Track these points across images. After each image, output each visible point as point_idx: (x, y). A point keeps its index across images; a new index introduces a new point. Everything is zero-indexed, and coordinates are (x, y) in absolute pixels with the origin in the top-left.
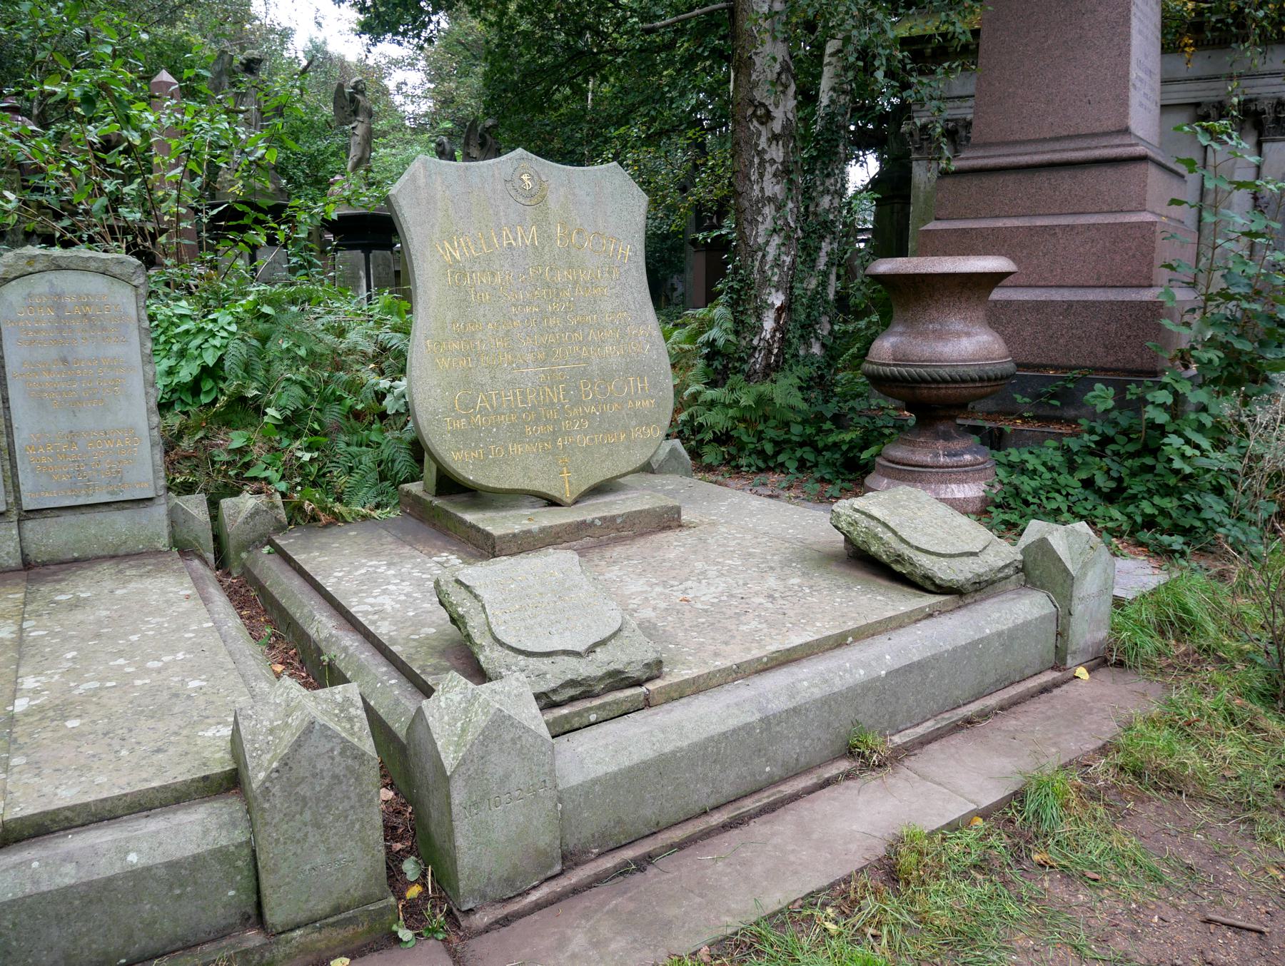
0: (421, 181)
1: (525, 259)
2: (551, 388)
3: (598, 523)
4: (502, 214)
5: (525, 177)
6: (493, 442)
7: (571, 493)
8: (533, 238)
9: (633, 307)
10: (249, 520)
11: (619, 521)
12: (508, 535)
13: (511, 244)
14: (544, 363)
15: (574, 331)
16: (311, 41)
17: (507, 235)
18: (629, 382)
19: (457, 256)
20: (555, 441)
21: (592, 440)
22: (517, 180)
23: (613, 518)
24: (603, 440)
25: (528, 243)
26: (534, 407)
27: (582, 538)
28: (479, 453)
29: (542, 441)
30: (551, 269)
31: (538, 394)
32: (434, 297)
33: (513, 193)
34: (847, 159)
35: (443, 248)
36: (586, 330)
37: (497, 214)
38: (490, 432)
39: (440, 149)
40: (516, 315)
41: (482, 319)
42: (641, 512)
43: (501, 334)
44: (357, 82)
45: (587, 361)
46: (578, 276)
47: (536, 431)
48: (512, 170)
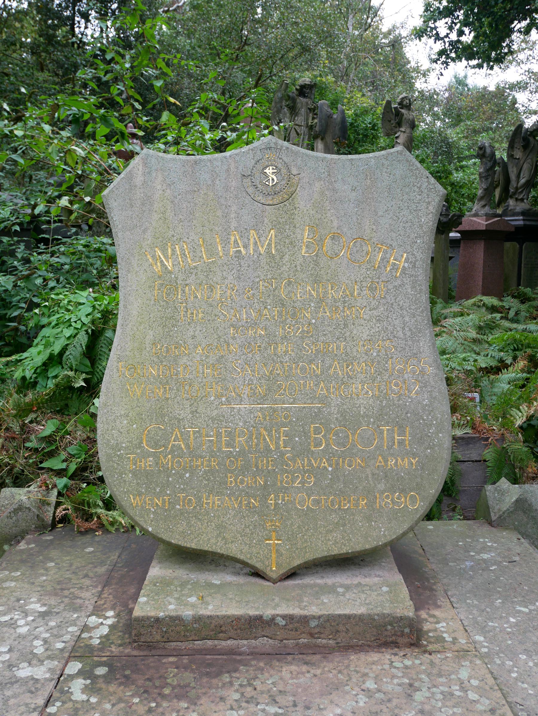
0: (139, 180)
1: (255, 270)
2: (269, 432)
3: (279, 620)
4: (233, 216)
5: (269, 171)
6: (183, 490)
7: (278, 565)
8: (269, 245)
9: (400, 334)
10: (12, 515)
11: (313, 624)
12: (148, 618)
13: (240, 251)
14: (263, 399)
15: (311, 362)
16: (455, 77)
17: (236, 241)
18: (382, 432)
19: (169, 265)
20: (265, 498)
21: (317, 502)
22: (257, 175)
23: (305, 620)
24: (333, 505)
25: (262, 250)
26: (242, 453)
27: (256, 638)
28: (164, 501)
29: (248, 495)
30: (289, 283)
31: (250, 437)
32: (135, 313)
33: (251, 190)
34: (490, 92)
35: (154, 257)
36: (328, 362)
37: (226, 216)
38: (182, 476)
39: (481, 152)
40: (234, 338)
41: (190, 341)
42: (348, 617)
43: (212, 360)
44: (403, 98)
45: (324, 400)
46: (326, 293)
47: (242, 482)
48: (253, 162)
